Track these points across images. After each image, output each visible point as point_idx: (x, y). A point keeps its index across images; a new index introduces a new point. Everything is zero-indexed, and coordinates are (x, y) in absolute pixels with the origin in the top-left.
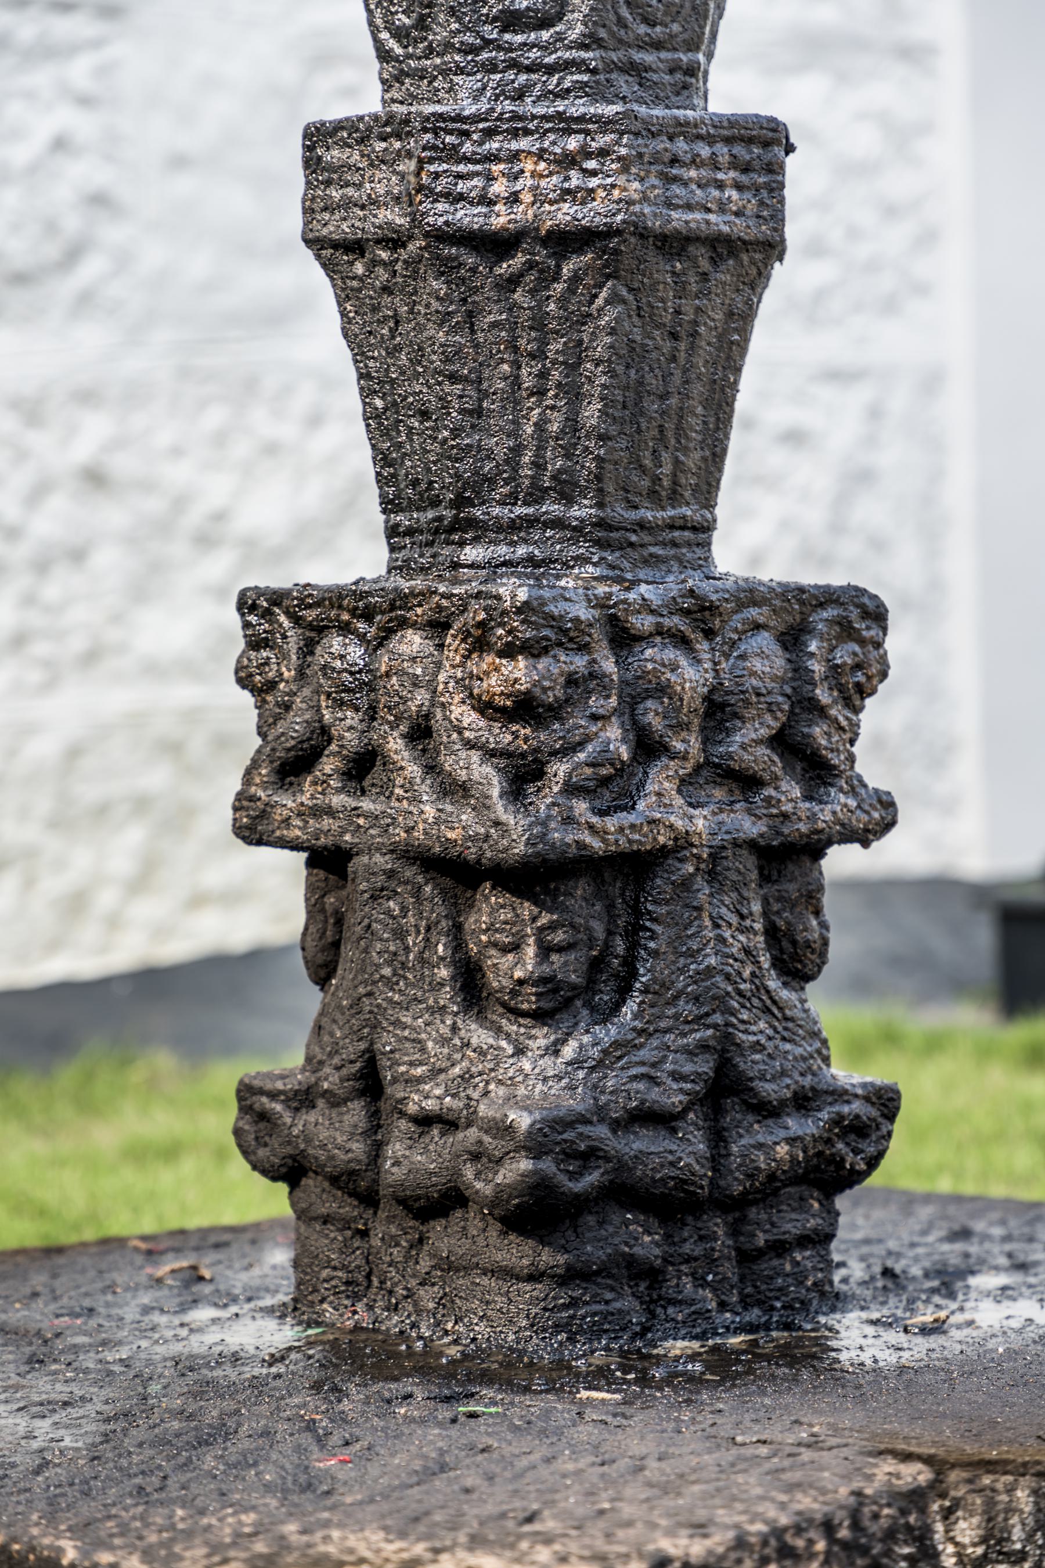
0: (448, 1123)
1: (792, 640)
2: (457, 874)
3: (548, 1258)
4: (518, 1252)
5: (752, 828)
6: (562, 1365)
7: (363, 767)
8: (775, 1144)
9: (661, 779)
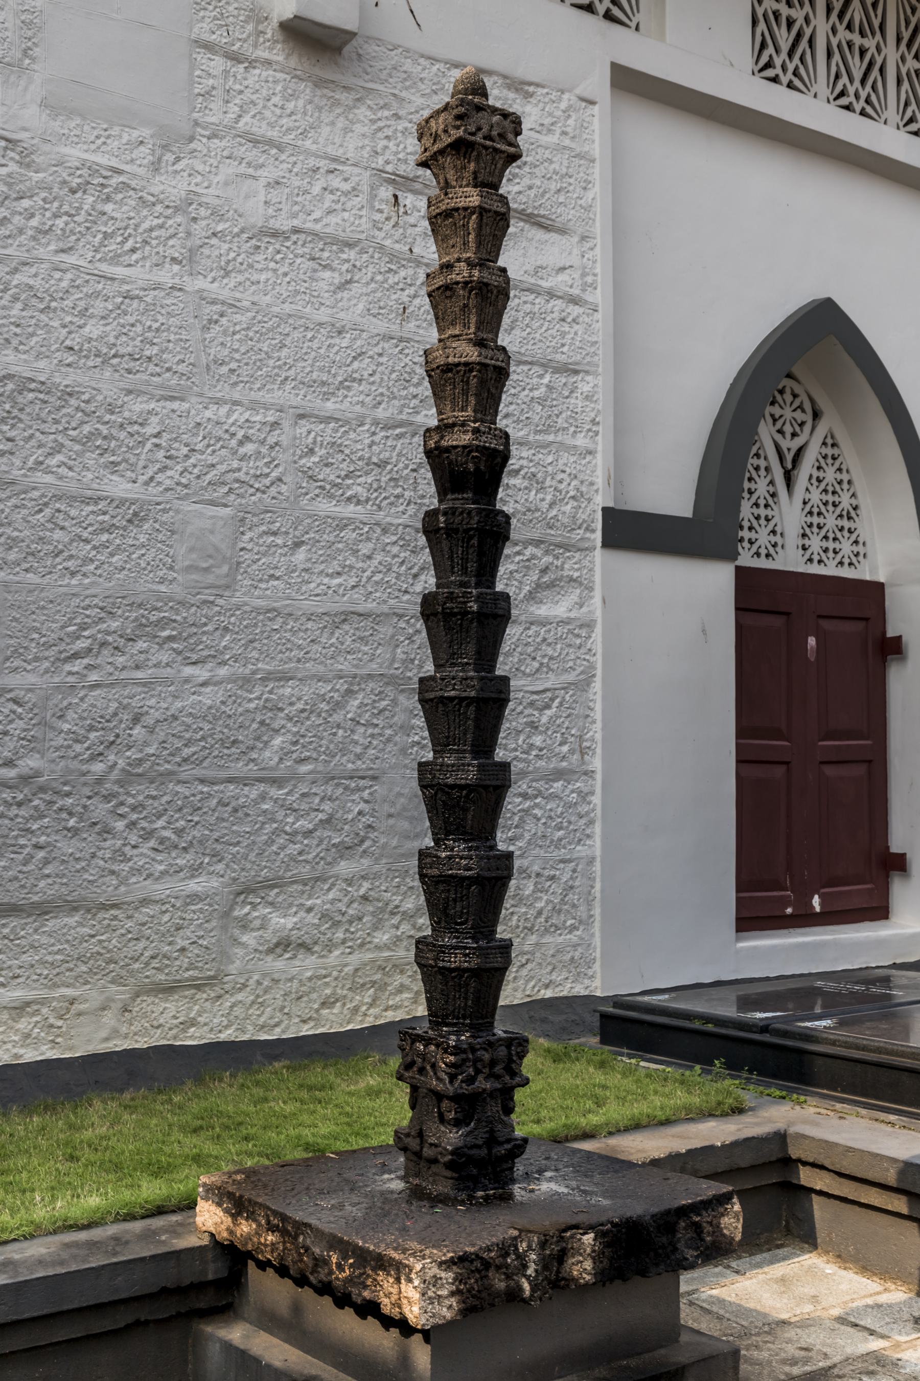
0: (436, 1146)
1: (509, 1047)
2: (439, 1097)
3: (454, 1175)
4: (449, 1173)
5: (499, 1086)
6: (456, 1199)
7: (422, 1071)
8: (502, 1150)
9: (480, 1078)
